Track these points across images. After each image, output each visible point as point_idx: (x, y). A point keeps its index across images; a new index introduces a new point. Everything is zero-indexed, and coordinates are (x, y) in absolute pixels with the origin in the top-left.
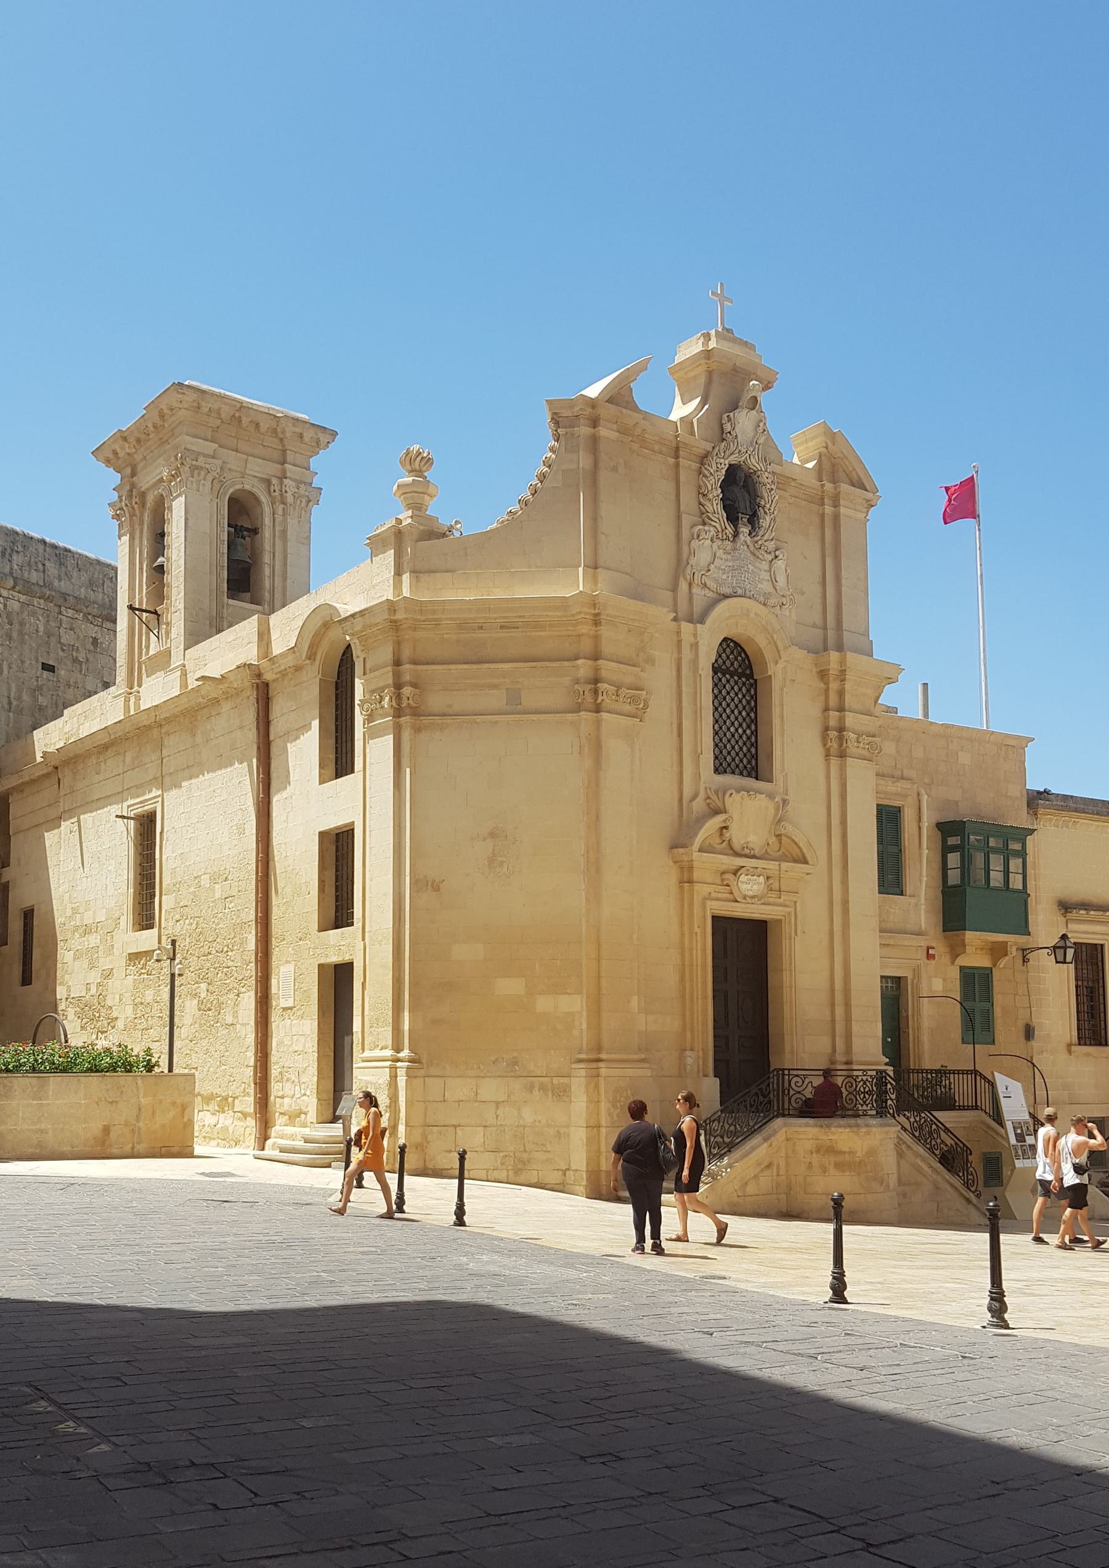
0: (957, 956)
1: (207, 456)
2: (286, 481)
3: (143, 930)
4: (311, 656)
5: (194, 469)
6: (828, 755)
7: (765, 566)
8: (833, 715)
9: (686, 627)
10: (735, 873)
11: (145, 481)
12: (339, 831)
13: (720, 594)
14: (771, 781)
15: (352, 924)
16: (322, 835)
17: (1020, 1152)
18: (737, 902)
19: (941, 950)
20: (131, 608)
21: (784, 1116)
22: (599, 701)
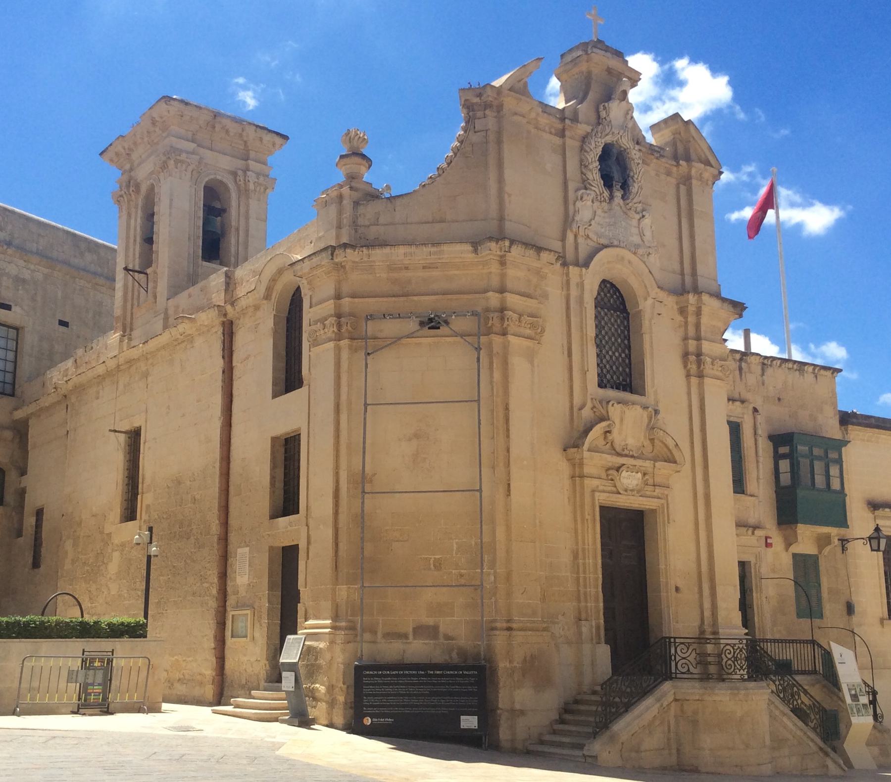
0: (790, 545)
1: (188, 153)
2: (249, 173)
3: (127, 521)
4: (267, 297)
5: (177, 162)
6: (688, 376)
7: (634, 222)
8: (692, 344)
9: (573, 270)
10: (618, 469)
11: (141, 174)
12: (287, 437)
13: (599, 244)
14: (642, 394)
15: (297, 512)
16: (274, 440)
17: (855, 710)
18: (620, 494)
19: (777, 540)
20: (126, 269)
21: (671, 679)
22: (505, 326)
